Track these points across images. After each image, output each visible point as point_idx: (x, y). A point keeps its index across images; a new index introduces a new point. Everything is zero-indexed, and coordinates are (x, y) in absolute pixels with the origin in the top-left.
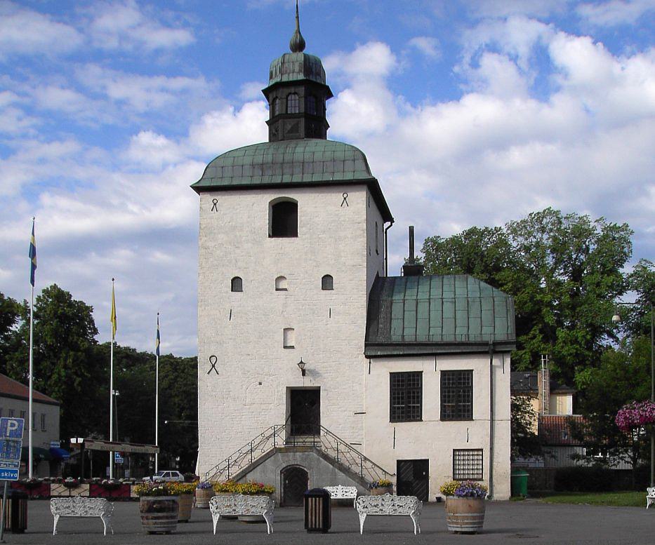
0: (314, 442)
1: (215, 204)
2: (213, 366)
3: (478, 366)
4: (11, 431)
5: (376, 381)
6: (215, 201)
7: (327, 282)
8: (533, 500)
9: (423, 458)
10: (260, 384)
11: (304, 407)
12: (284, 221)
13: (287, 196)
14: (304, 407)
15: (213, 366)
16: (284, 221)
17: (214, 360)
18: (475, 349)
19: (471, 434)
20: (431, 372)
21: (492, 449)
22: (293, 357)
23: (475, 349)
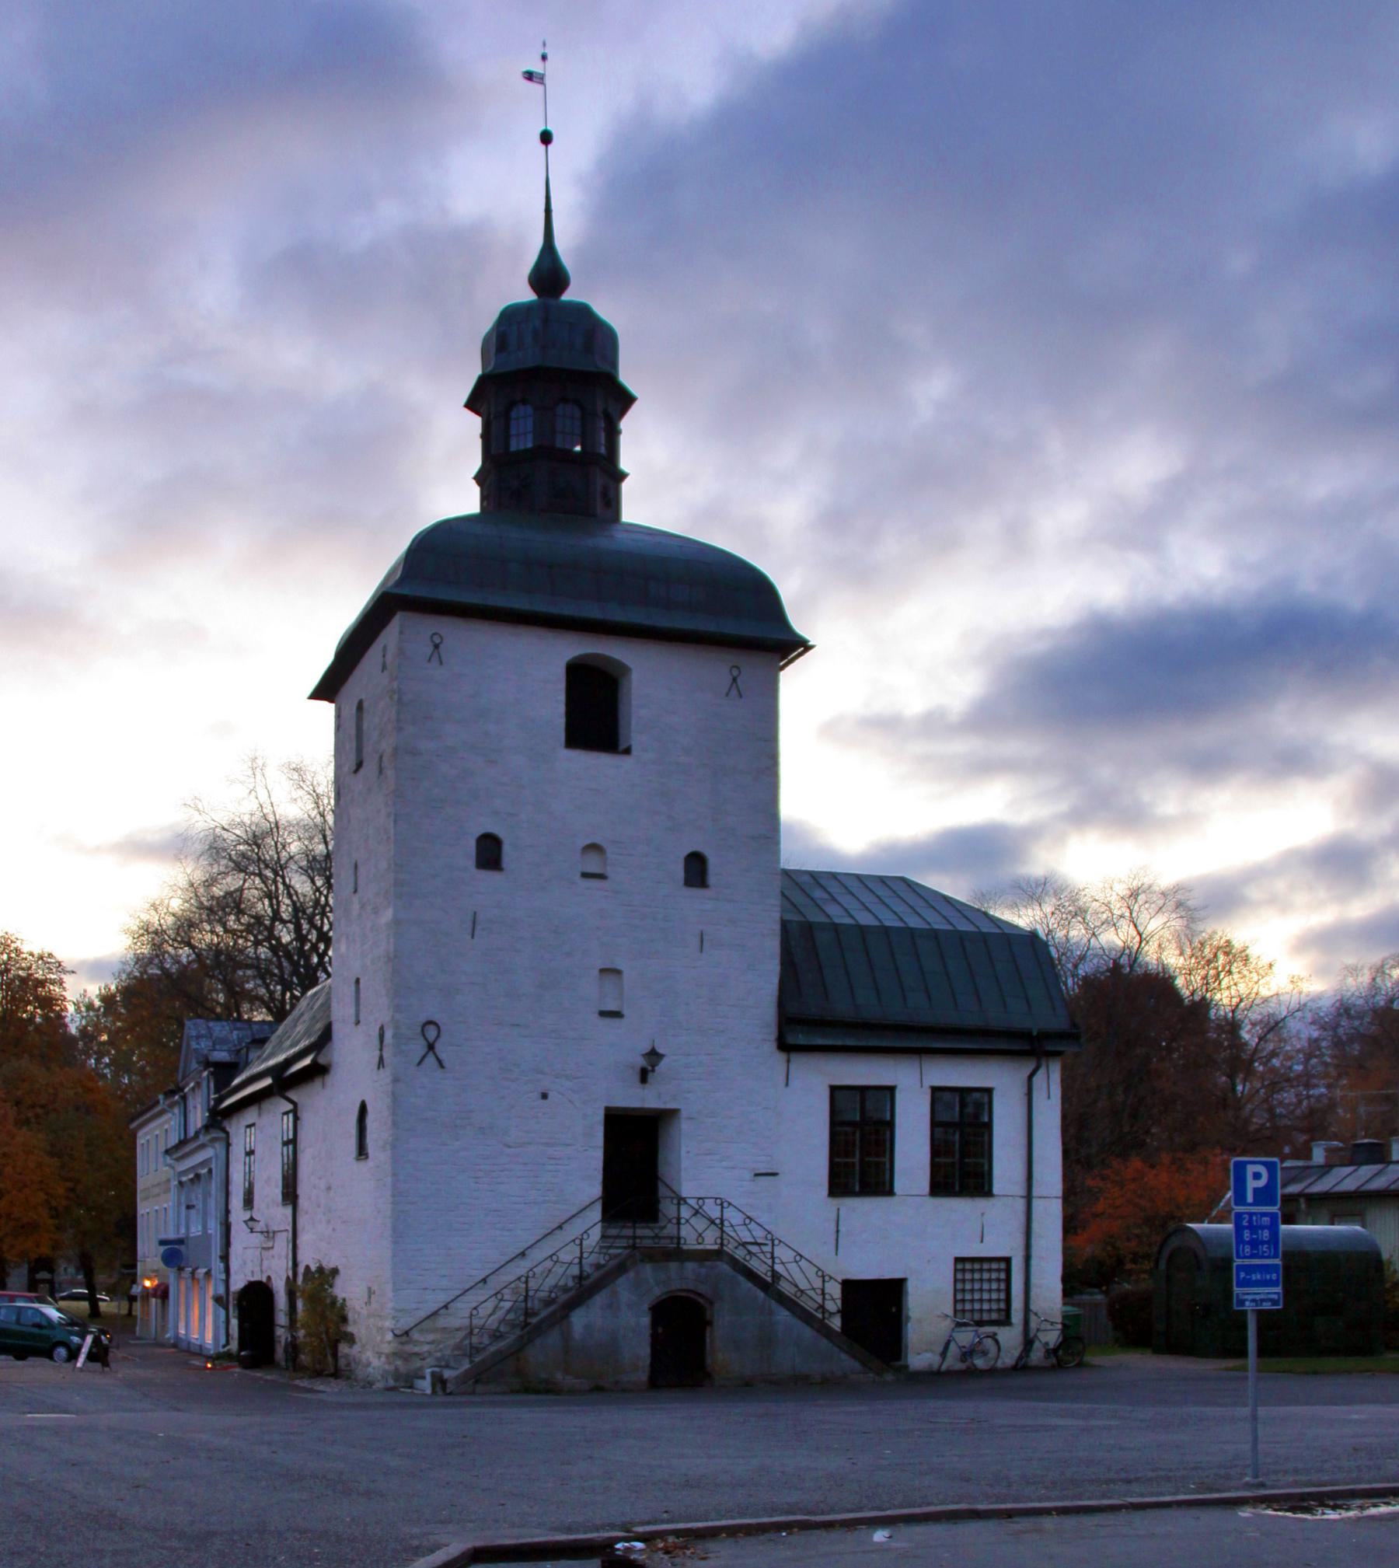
0: (635, 1237)
1: (437, 646)
2: (431, 1047)
3: (1001, 1081)
4: (1256, 1191)
5: (796, 1108)
6: (437, 640)
7: (696, 870)
8: (1142, 1363)
9: (888, 1276)
10: (544, 1096)
11: (635, 1149)
12: (594, 714)
13: (607, 653)
14: (635, 1149)
15: (431, 1047)
16: (594, 714)
17: (431, 1033)
18: (1003, 1045)
19: (985, 1226)
20: (912, 1090)
21: (1028, 1258)
22: (623, 1044)
23: (1003, 1045)
